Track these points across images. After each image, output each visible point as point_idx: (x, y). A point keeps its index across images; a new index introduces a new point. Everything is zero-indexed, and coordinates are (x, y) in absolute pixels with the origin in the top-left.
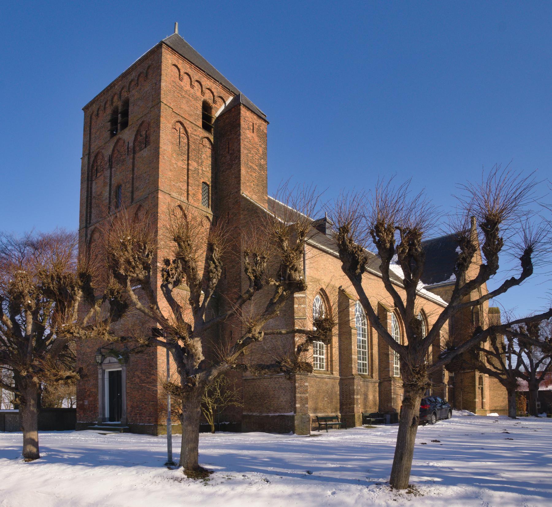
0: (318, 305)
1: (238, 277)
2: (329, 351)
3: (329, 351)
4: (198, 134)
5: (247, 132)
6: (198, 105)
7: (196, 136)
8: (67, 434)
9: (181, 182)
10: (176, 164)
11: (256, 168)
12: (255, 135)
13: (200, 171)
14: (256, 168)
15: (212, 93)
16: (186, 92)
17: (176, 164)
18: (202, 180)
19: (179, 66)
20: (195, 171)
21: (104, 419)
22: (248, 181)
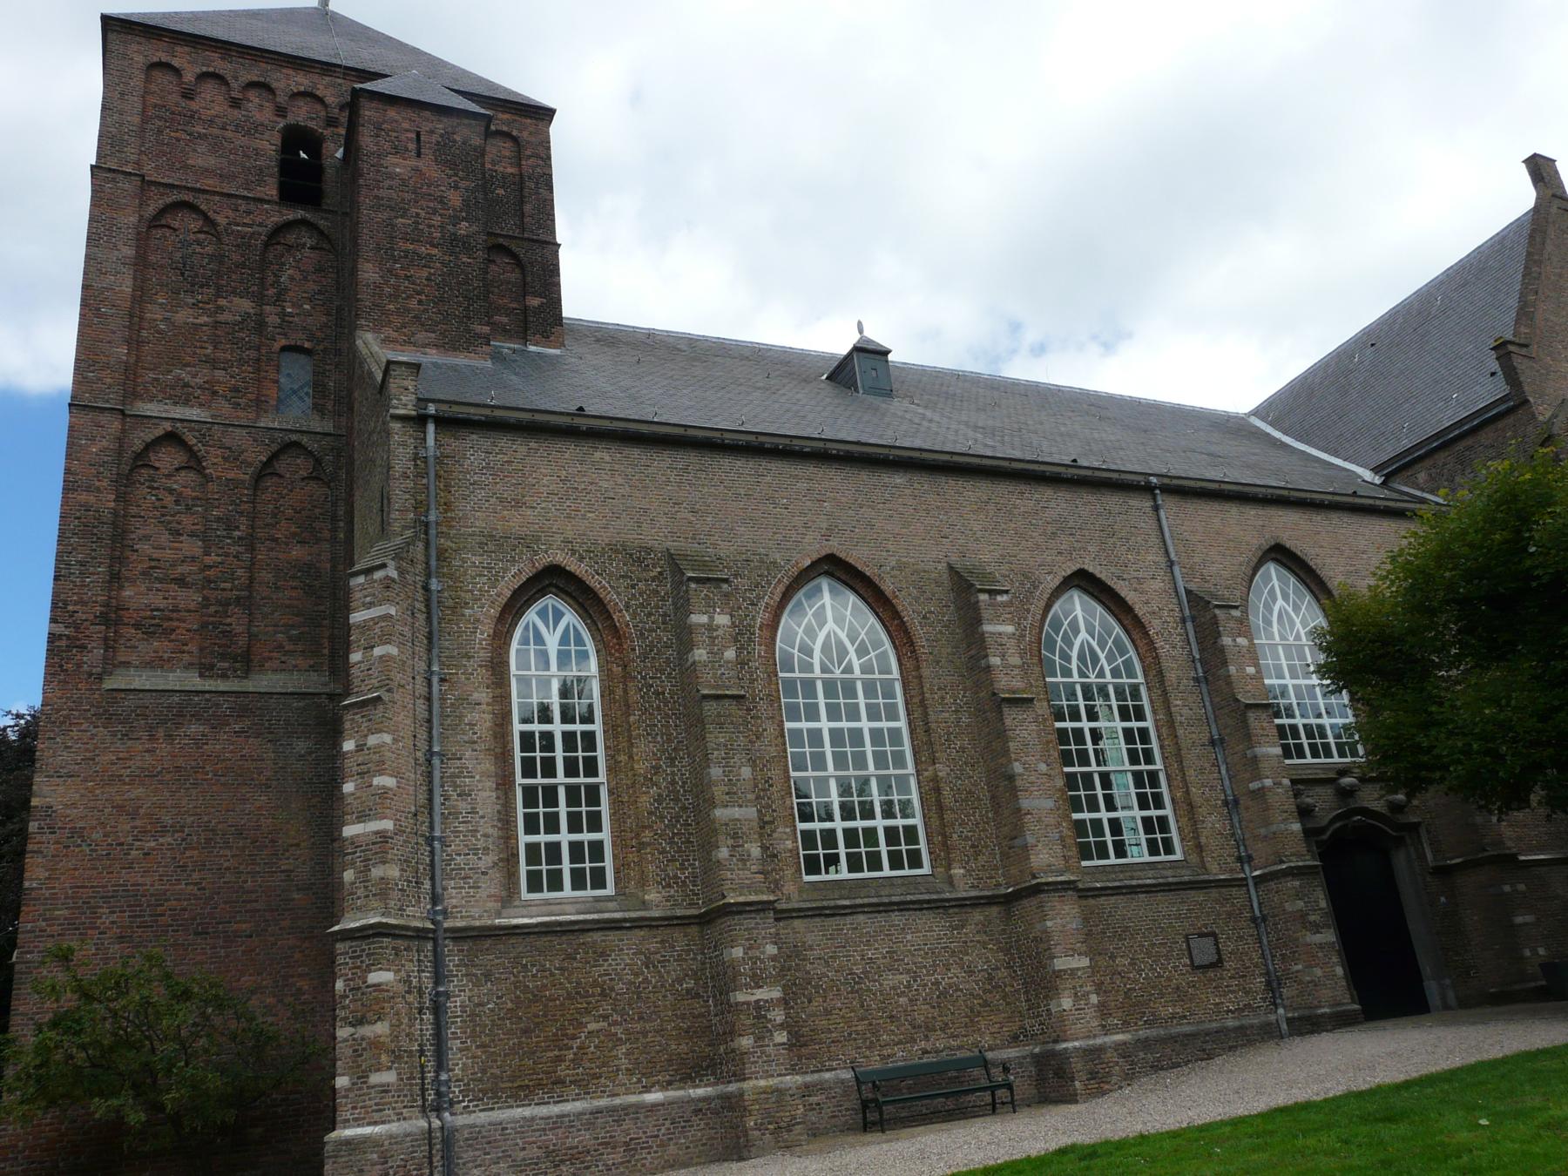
4: (258, 220)
7: (250, 226)
12: (428, 165)
15: (320, 100)
19: (176, 62)
22: (394, 297)
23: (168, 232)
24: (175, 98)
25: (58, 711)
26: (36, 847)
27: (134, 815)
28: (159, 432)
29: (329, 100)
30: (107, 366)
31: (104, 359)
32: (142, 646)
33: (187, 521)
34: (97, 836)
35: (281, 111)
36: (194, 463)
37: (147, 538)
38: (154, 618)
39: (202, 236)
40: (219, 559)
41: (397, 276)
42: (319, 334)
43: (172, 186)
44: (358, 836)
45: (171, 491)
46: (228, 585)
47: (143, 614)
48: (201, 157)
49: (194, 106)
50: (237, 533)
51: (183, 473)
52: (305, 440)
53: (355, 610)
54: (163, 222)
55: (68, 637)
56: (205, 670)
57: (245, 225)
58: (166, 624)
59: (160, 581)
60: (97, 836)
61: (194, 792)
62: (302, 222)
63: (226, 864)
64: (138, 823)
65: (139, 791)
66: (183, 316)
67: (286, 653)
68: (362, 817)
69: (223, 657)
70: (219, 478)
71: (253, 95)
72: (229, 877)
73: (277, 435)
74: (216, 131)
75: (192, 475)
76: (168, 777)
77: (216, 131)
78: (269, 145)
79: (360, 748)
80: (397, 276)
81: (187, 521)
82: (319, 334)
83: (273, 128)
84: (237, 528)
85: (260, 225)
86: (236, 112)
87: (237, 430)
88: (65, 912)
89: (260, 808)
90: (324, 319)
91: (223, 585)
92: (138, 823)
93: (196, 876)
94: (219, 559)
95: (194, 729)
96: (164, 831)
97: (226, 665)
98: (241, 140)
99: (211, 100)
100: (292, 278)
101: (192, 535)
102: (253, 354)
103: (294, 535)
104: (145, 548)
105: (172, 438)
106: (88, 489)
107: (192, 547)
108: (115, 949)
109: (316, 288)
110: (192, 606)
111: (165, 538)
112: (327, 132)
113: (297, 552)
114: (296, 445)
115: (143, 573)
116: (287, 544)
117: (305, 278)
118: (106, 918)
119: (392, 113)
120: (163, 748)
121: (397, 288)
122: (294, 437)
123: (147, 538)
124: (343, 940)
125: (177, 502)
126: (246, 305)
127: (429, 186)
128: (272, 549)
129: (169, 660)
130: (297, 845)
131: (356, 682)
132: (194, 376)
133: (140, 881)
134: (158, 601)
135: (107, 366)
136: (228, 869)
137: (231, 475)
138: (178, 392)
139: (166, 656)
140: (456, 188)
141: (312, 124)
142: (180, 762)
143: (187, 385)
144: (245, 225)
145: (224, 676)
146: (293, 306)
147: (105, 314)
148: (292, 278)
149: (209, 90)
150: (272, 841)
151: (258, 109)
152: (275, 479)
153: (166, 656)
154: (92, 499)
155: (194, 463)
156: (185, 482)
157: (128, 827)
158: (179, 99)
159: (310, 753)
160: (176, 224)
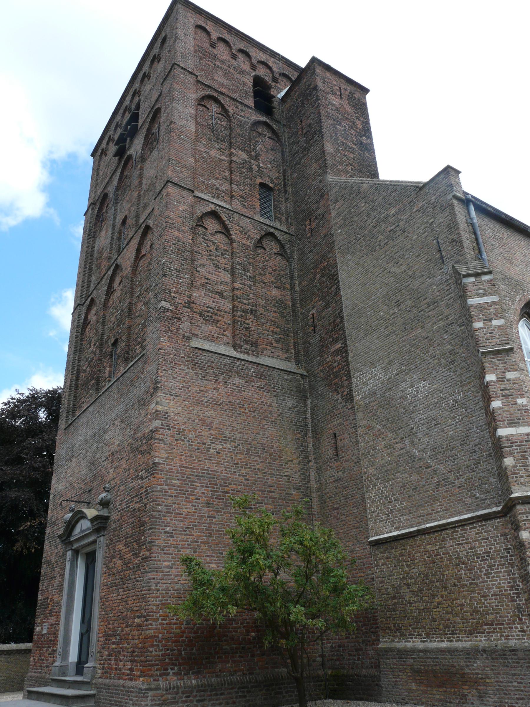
0: (493, 532)
1: (338, 320)
2: (469, 522)
3: (469, 522)
4: (247, 116)
5: (330, 96)
6: (246, 80)
7: (244, 117)
8: (15, 696)
9: (217, 178)
10: (206, 152)
11: (354, 147)
12: (345, 102)
13: (255, 167)
14: (354, 147)
15: (270, 68)
16: (223, 62)
17: (206, 152)
18: (259, 181)
19: (208, 28)
20: (243, 163)
21: (63, 670)
22: (341, 163)
23: (205, 109)
24: (207, 45)
25: (169, 354)
26: (160, 437)
27: (210, 427)
28: (208, 209)
29: (274, 69)
30: (184, 166)
31: (184, 163)
32: (203, 327)
33: (222, 262)
34: (192, 436)
35: (253, 67)
36: (226, 231)
37: (203, 265)
38: (208, 312)
39: (220, 116)
40: (241, 286)
41: (341, 153)
42: (275, 181)
43: (209, 87)
44: (512, 435)
45: (214, 243)
46: (246, 302)
47: (203, 308)
48: (219, 77)
49: (216, 52)
50: (248, 274)
51: (219, 235)
52: (276, 233)
53: (470, 297)
54: (203, 103)
55: (172, 312)
56: (235, 347)
57: (241, 116)
58: (215, 317)
59: (211, 292)
60: (192, 436)
61: (239, 419)
62: (265, 124)
63: (258, 467)
64: (212, 432)
65: (211, 413)
66: (214, 153)
67: (274, 347)
68: (512, 424)
69: (246, 342)
70: (238, 241)
71: (240, 55)
72: (260, 475)
73: (263, 226)
74: (226, 67)
75: (223, 237)
76: (226, 407)
77: (226, 67)
78: (249, 81)
79: (501, 380)
80: (341, 153)
81: (222, 262)
82: (275, 181)
83: (250, 75)
84: (248, 271)
85: (248, 118)
86: (234, 61)
87: (246, 219)
88: (177, 482)
89: (272, 435)
90: (277, 174)
91: (244, 301)
92: (212, 432)
93: (243, 471)
94: (241, 286)
95: (237, 381)
96: (225, 440)
97: (248, 347)
98: (237, 75)
99: (221, 50)
100: (261, 148)
101: (225, 270)
102: (249, 181)
103: (273, 283)
104: (202, 271)
105: (214, 214)
106: (179, 230)
107: (226, 277)
108: (205, 510)
109: (273, 158)
110: (227, 309)
111: (212, 268)
112: (273, 84)
113: (275, 292)
114: (272, 234)
115: (202, 285)
116: (270, 287)
117: (267, 151)
118: (199, 491)
119: (328, 75)
120: (223, 389)
121: (341, 159)
122: (272, 230)
123: (203, 265)
124: (523, 503)
125: (217, 250)
126: (244, 156)
127: (348, 115)
128: (263, 288)
129: (217, 338)
130: (292, 461)
131: (482, 340)
132: (221, 185)
133: (216, 469)
134: (210, 303)
135: (184, 166)
136: (258, 469)
137: (244, 242)
138: (214, 191)
139: (216, 335)
140: (359, 120)
141: (266, 78)
142: (231, 399)
143: (217, 189)
144: (241, 116)
145: (247, 353)
146: (263, 164)
147: (183, 139)
148: (261, 148)
149: (221, 46)
150: (279, 456)
151: (243, 63)
152: (262, 250)
153: (216, 335)
154: (181, 236)
155: (226, 231)
156: (220, 239)
157: (207, 434)
158: (209, 46)
159: (294, 407)
160: (208, 106)
